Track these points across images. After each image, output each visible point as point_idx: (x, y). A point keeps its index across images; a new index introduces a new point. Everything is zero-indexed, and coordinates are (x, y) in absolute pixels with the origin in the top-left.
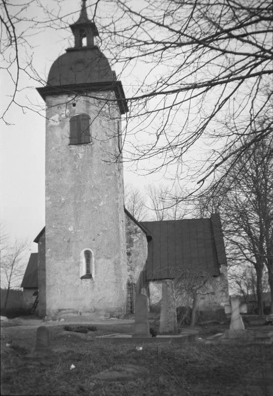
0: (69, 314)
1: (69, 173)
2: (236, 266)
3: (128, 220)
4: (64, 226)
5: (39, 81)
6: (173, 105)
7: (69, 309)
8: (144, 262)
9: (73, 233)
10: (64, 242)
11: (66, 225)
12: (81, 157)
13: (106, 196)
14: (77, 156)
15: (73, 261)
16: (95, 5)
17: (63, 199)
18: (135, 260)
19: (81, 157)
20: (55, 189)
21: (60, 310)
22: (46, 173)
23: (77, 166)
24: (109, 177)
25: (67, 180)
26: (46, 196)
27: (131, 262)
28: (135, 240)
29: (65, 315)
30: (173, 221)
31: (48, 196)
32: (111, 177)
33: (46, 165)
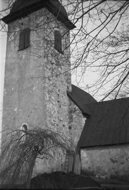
1: (17, 70)
2: (55, 157)
3: (70, 101)
4: (13, 108)
8: (80, 134)
9: (17, 112)
10: (12, 119)
11: (13, 107)
12: (24, 58)
13: (37, 82)
14: (22, 58)
17: (13, 89)
18: (74, 132)
19: (24, 58)
20: (9, 83)
22: (5, 73)
23: (21, 64)
24: (39, 68)
25: (15, 76)
26: (4, 88)
27: (71, 134)
28: (74, 117)
30: (91, 96)
31: (5, 88)
32: (41, 68)
33: (5, 67)
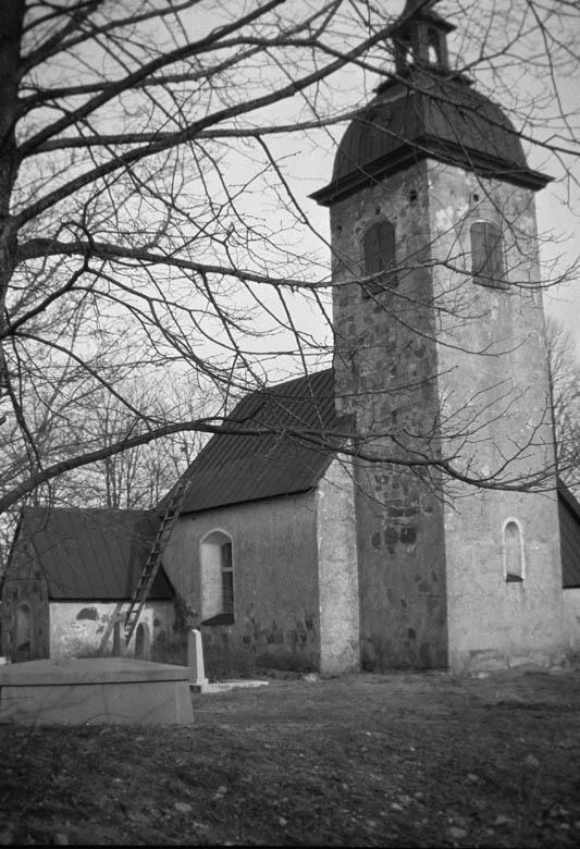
0: (491, 662)
5: (547, 120)
6: (293, 329)
7: (489, 651)
15: (492, 542)
16: (508, 52)
21: (473, 654)
23: (489, 334)
29: (484, 663)
